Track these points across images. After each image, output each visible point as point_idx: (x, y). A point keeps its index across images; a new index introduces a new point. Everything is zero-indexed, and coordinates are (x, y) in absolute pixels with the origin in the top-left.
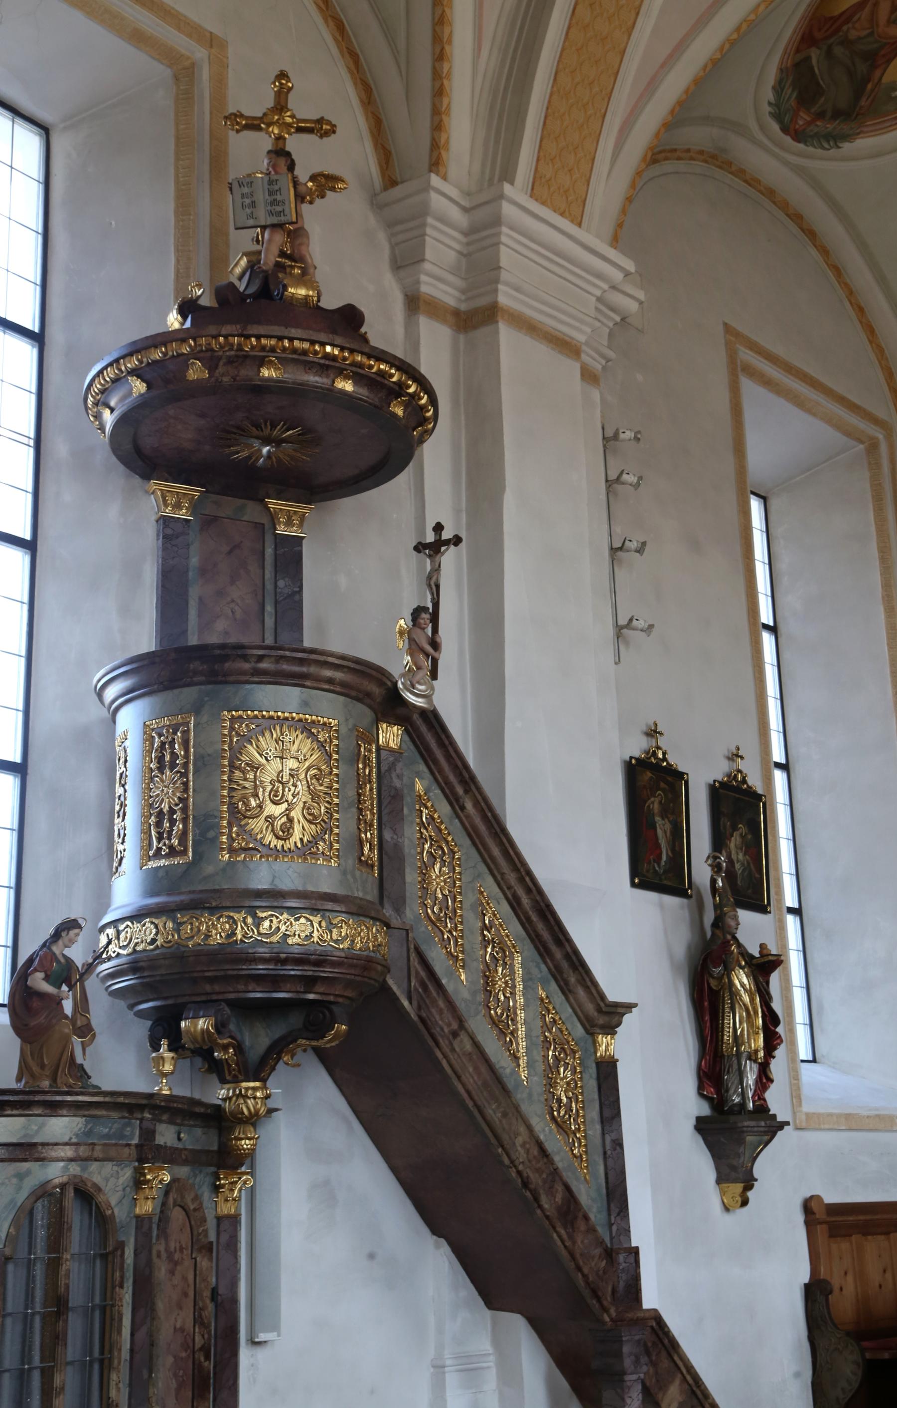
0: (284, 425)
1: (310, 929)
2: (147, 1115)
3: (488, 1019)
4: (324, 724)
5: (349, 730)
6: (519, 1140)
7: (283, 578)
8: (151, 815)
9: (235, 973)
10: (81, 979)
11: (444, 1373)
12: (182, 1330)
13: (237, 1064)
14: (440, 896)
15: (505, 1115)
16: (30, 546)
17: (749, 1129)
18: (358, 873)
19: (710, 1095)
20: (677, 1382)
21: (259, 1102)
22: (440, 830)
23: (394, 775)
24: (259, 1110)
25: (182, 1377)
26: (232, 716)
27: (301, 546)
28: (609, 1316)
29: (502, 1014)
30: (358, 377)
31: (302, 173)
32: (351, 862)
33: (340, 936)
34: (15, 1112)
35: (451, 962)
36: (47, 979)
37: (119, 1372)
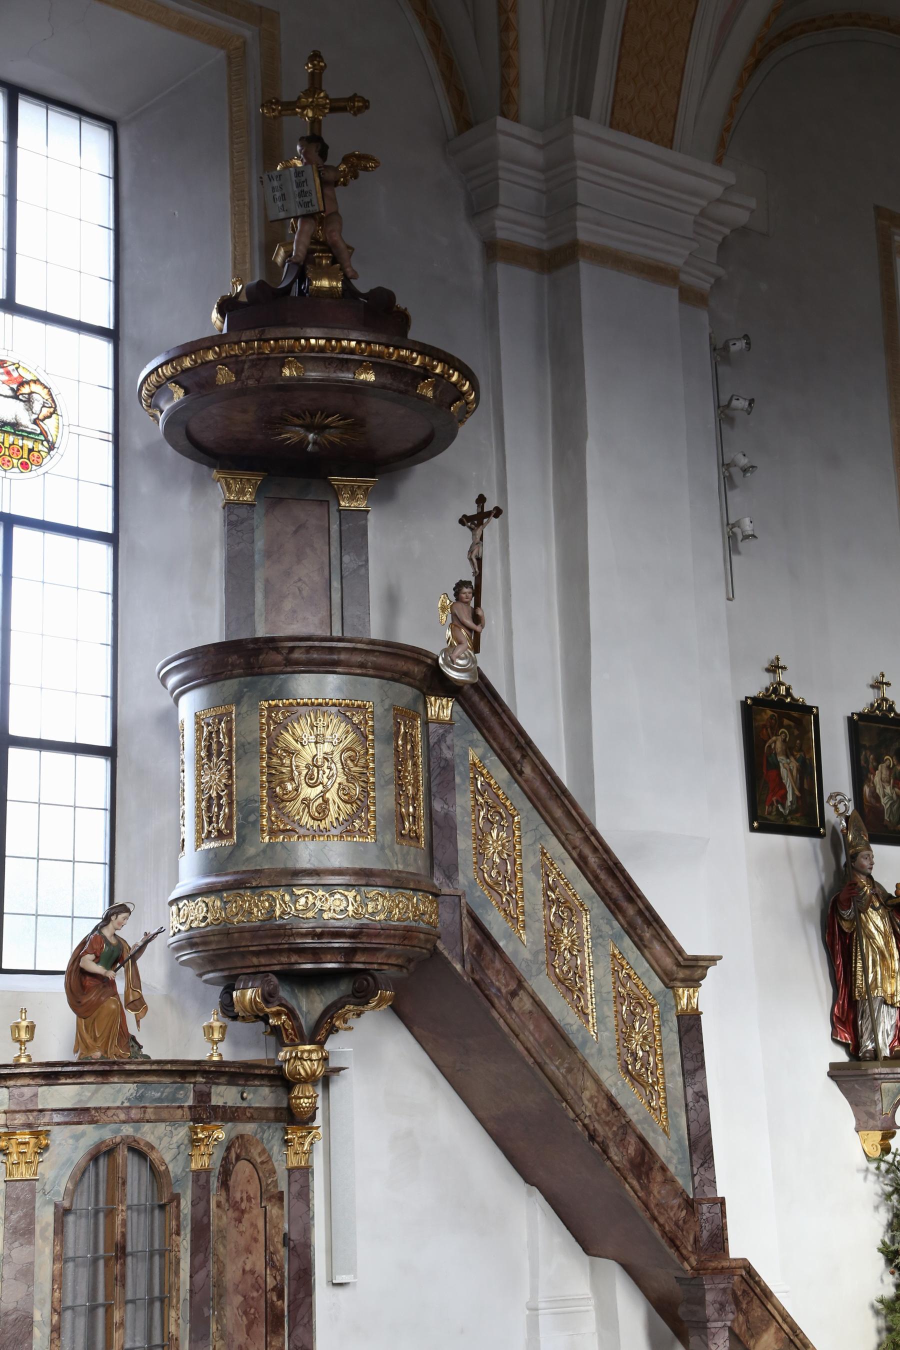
0: (322, 414)
1: (344, 904)
2: (200, 1079)
3: (553, 978)
4: (359, 707)
5: (385, 710)
6: (586, 1095)
7: (348, 554)
8: (203, 800)
9: (276, 947)
10: (134, 957)
11: (537, 1315)
12: (252, 1272)
13: (293, 1029)
14: (498, 860)
15: (570, 1070)
16: (111, 539)
17: (882, 1076)
18: (397, 847)
19: (844, 1041)
20: (772, 1330)
21: (316, 1063)
22: (498, 796)
23: (444, 746)
24: (315, 1071)
25: (254, 1314)
26: (269, 704)
27: (366, 519)
28: (690, 1265)
29: (569, 972)
30: (377, 367)
31: (334, 159)
32: (388, 837)
33: (376, 908)
34: (69, 1081)
35: (510, 924)
36: (97, 960)
37: (178, 1309)
